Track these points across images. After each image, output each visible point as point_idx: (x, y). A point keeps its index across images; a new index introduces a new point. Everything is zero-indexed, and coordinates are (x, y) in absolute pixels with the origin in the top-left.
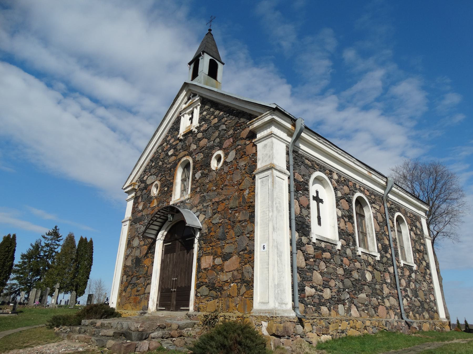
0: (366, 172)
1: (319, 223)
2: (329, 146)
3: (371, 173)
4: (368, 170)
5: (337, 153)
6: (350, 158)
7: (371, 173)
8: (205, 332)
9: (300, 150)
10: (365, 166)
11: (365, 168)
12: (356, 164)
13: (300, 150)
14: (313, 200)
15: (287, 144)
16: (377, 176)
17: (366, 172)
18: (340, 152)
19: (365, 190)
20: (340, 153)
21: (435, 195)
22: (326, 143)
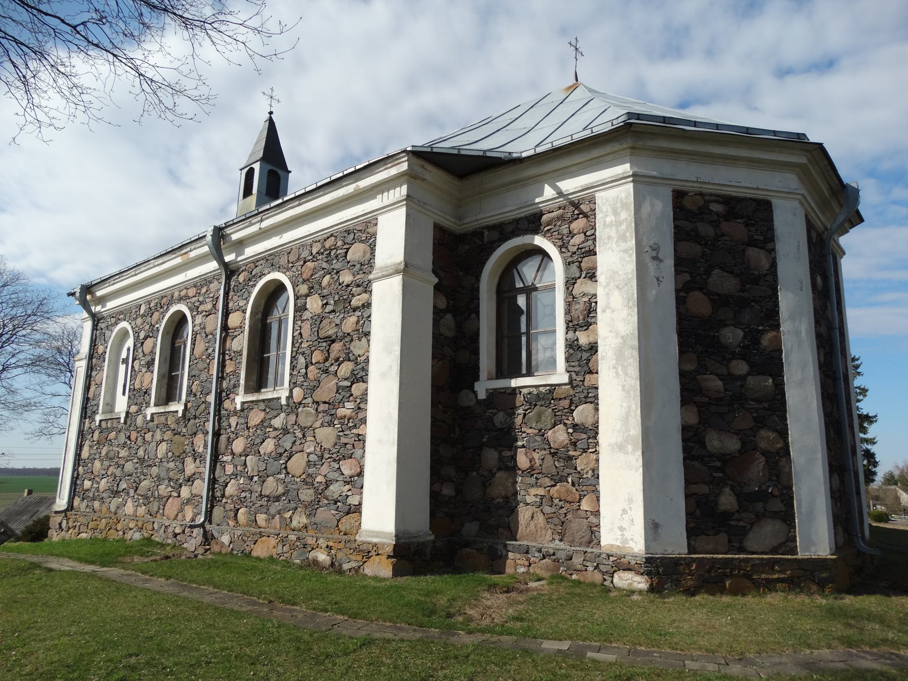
0: (178, 260)
1: (801, 282)
2: (122, 279)
3: (187, 252)
4: (179, 253)
5: (132, 276)
6: (147, 267)
7: (187, 252)
8: (51, 44)
9: (540, 206)
10: (170, 255)
11: (174, 256)
12: (158, 265)
13: (540, 206)
14: (857, 191)
15: (807, 210)
16: (197, 246)
17: (178, 260)
18: (132, 272)
19: (17, 363)
20: (133, 273)
21: (14, 312)
22: (116, 279)
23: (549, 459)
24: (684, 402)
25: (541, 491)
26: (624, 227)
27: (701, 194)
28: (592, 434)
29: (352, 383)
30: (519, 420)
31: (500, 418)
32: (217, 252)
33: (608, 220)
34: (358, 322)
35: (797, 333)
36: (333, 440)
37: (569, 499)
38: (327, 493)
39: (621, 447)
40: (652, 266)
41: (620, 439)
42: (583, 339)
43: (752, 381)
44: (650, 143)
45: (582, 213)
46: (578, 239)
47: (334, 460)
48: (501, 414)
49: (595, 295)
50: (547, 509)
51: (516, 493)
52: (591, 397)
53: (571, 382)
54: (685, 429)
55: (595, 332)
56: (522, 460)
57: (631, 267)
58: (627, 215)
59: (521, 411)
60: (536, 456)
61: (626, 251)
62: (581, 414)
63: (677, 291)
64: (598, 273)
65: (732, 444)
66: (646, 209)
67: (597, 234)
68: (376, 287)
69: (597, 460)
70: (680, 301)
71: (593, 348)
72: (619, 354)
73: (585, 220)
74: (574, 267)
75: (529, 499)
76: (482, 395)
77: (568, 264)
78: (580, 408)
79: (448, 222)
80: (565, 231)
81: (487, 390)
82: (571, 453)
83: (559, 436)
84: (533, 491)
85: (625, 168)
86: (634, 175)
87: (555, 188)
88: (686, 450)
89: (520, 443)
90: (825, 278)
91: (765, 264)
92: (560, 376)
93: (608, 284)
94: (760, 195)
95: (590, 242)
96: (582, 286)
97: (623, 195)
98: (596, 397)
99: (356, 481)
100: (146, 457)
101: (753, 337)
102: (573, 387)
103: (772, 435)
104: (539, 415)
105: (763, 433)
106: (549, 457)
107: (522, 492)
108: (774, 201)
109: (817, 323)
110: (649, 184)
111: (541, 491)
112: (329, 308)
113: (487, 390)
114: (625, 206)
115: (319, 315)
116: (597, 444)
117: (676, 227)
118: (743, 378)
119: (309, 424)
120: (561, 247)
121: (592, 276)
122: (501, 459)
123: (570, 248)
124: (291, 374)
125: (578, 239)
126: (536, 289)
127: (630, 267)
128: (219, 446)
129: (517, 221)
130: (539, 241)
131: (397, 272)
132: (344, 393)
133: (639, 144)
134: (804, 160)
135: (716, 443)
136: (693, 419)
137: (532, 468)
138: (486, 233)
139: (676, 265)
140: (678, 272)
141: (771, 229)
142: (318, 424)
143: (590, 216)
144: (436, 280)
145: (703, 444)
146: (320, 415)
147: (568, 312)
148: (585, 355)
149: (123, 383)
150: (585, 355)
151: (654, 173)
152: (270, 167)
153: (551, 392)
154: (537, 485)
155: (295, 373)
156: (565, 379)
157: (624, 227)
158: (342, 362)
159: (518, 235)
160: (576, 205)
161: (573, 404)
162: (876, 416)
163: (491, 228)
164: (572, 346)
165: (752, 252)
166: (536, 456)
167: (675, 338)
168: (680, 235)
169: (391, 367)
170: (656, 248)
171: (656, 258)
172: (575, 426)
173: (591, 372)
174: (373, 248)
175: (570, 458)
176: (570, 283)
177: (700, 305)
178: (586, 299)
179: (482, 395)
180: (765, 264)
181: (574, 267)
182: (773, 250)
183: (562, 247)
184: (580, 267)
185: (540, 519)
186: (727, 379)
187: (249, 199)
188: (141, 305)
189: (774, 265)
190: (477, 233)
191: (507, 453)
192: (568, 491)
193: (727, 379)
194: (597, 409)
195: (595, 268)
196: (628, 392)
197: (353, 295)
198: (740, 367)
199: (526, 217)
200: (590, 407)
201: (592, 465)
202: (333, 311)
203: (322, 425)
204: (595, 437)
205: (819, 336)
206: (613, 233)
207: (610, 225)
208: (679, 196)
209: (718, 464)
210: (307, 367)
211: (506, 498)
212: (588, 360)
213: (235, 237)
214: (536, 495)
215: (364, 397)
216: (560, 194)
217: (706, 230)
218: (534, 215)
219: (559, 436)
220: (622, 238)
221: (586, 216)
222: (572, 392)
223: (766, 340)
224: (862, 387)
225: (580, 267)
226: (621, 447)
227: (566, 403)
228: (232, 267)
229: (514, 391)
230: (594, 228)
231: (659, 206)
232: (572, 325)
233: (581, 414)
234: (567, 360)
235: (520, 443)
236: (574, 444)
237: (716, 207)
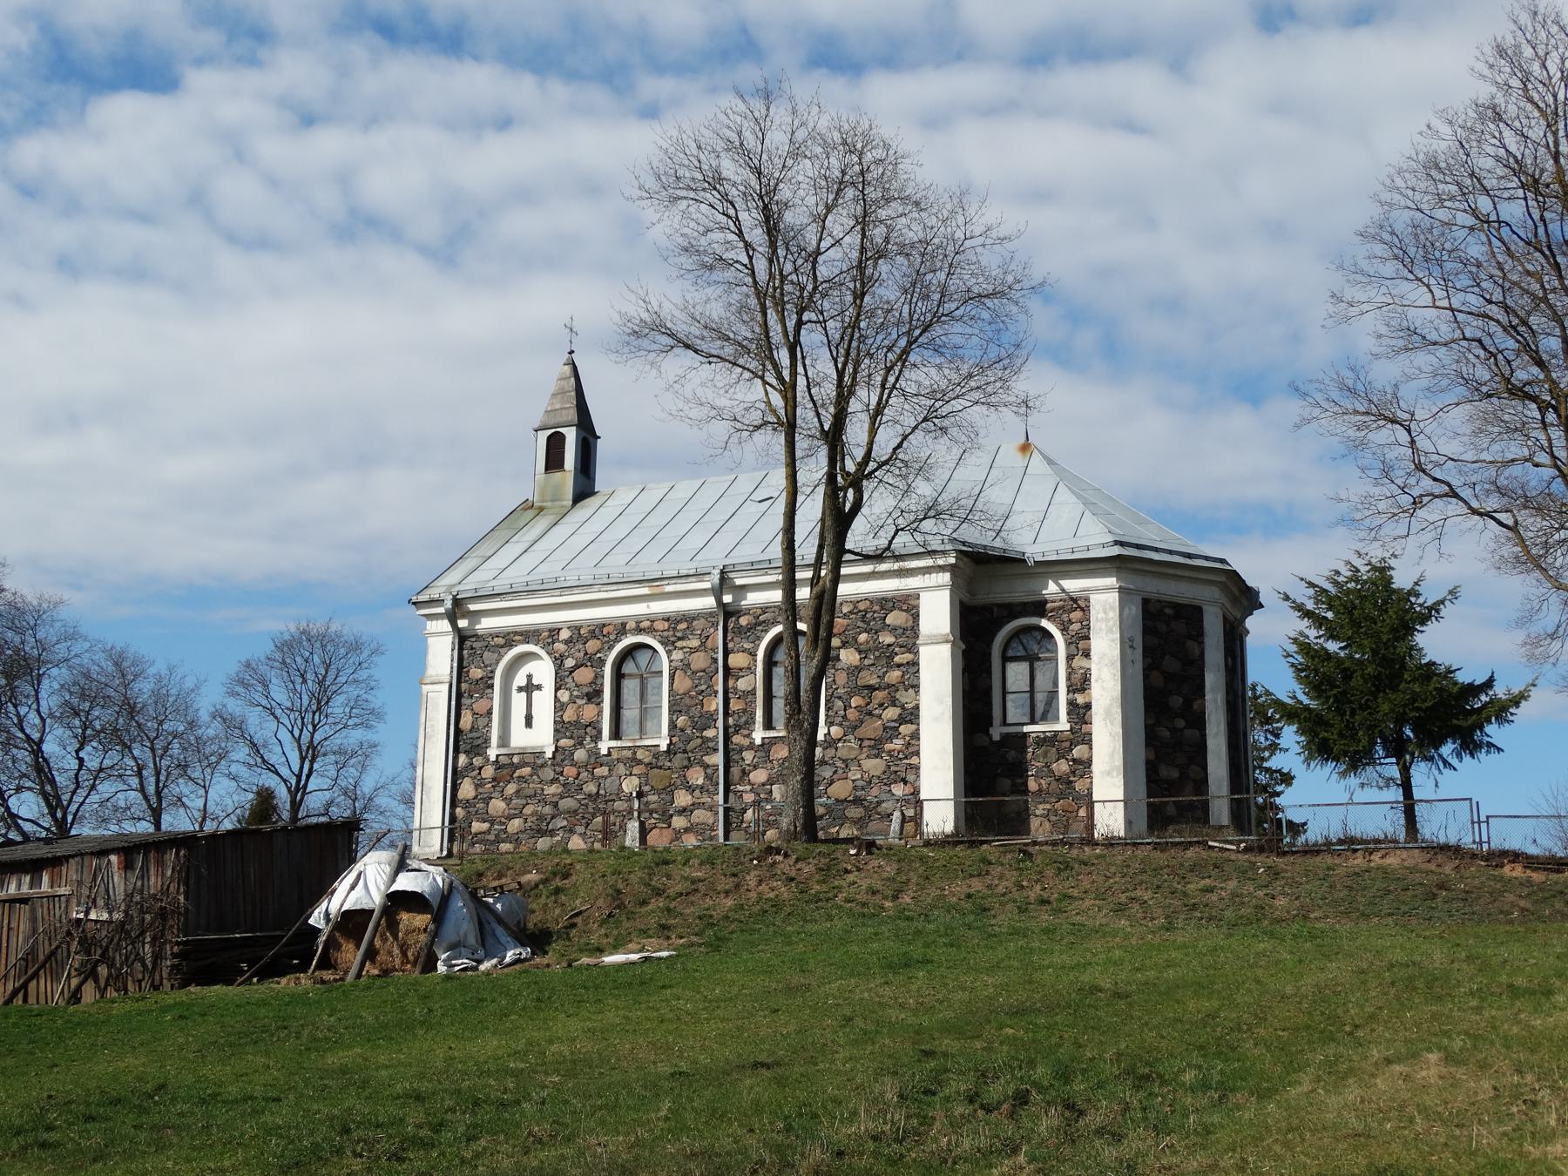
18: (557, 592)
23: (1054, 784)
24: (1147, 745)
25: (1048, 806)
26: (1111, 623)
27: (1159, 601)
28: (1087, 765)
29: (900, 724)
30: (1029, 756)
31: (1011, 755)
32: (718, 592)
33: (1100, 616)
34: (903, 676)
35: (1216, 700)
36: (883, 768)
37: (1070, 809)
38: (879, 809)
39: (1109, 773)
40: (1129, 651)
41: (1108, 768)
42: (1080, 699)
43: (1188, 732)
44: (1129, 566)
45: (1079, 607)
46: (1075, 627)
47: (885, 784)
48: (1013, 752)
49: (1090, 669)
50: (1053, 818)
51: (1027, 809)
52: (1087, 740)
53: (1071, 730)
54: (1148, 762)
55: (1090, 695)
56: (1032, 785)
57: (1117, 652)
58: (1114, 615)
59: (1030, 750)
60: (1043, 782)
61: (1113, 641)
62: (1078, 752)
63: (1144, 670)
64: (1092, 653)
65: (1175, 774)
66: (1126, 611)
67: (1091, 625)
68: (922, 650)
69: (1092, 782)
70: (1146, 677)
71: (1088, 706)
72: (1108, 712)
73: (1081, 613)
74: (1073, 647)
75: (1038, 812)
76: (996, 737)
77: (1068, 644)
78: (1078, 747)
79: (965, 599)
80: (1066, 619)
81: (1001, 734)
82: (1071, 779)
83: (1062, 767)
84: (1041, 807)
85: (1114, 580)
86: (1120, 588)
87: (1059, 585)
88: (1148, 776)
89: (1030, 773)
90: (1234, 659)
91: (1197, 652)
92: (1063, 724)
93: (1100, 663)
94: (1195, 603)
95: (1086, 630)
96: (1079, 662)
97: (1111, 600)
98: (1091, 740)
99: (1084, 766)
100: (602, 792)
101: (1188, 703)
102: (1073, 733)
103: (1199, 769)
104: (1046, 754)
105: (1193, 767)
106: (1054, 782)
107: (1032, 808)
108: (1204, 607)
109: (1228, 693)
110: (1129, 594)
111: (1048, 806)
112: (867, 662)
113: (1001, 734)
114: (1112, 608)
115: (856, 667)
116: (1091, 772)
117: (1144, 625)
118: (1182, 730)
119: (852, 757)
120: (1062, 630)
121: (1087, 655)
122: (1014, 785)
123: (1070, 632)
124: (826, 715)
125: (1075, 627)
126: (1039, 659)
127: (1115, 652)
128: (731, 777)
129: (1025, 604)
130: (1045, 623)
131: (947, 642)
132: (891, 731)
133: (1123, 566)
134: (1224, 579)
135: (1165, 773)
136: (1152, 757)
137: (1040, 790)
138: (995, 610)
139: (1144, 652)
140: (1144, 657)
141: (1202, 627)
142: (864, 756)
143: (1085, 610)
144: (964, 647)
145: (1158, 773)
146: (865, 750)
147: (1068, 679)
148: (1082, 711)
149: (524, 713)
150: (1082, 711)
151: (1131, 587)
152: (584, 434)
153: (1055, 736)
154: (1044, 802)
155: (830, 713)
156: (1067, 727)
157: (1111, 623)
158: (887, 707)
159: (1025, 616)
160: (1074, 600)
161: (1073, 744)
162: (1305, 824)
163: (1000, 606)
164: (1072, 704)
165: (1190, 643)
166: (1043, 782)
167: (1142, 701)
168: (1147, 631)
169: (943, 714)
170: (1131, 640)
171: (1131, 647)
172: (1074, 760)
173: (1086, 723)
174: (916, 617)
175: (1071, 782)
176: (1070, 658)
177: (1158, 680)
178: (1082, 671)
179: (996, 737)
180: (1197, 652)
181: (1073, 647)
182: (1203, 642)
183: (1064, 630)
184: (1077, 648)
185: (1047, 825)
186: (1173, 730)
187: (557, 476)
188: (559, 629)
189: (1202, 654)
190: (988, 608)
191: (1020, 781)
192: (1070, 805)
193: (1173, 730)
194: (1091, 749)
195: (1090, 650)
196: (1114, 737)
197: (896, 654)
198: (1180, 723)
199: (1032, 602)
200: (1086, 747)
201: (1088, 786)
202: (873, 665)
203: (868, 757)
204: (1089, 767)
205: (1228, 703)
206: (1103, 626)
207: (1101, 620)
208: (1146, 602)
209: (1166, 786)
210: (845, 710)
211: (1019, 814)
212: (1085, 715)
213: (739, 582)
214: (1044, 809)
215: (916, 736)
216: (1063, 590)
217: (1162, 627)
218: (1040, 602)
219: (1062, 767)
220: (1110, 631)
221: (1082, 610)
222: (1072, 737)
223: (1196, 706)
224: (1285, 771)
225: (1077, 648)
226: (1109, 773)
227: (1067, 744)
228: (730, 609)
229: (1026, 735)
230: (1089, 620)
231: (1134, 609)
232: (1072, 689)
233: (1078, 752)
234: (1068, 714)
235: (1030, 773)
236: (1073, 773)
237: (1168, 611)
